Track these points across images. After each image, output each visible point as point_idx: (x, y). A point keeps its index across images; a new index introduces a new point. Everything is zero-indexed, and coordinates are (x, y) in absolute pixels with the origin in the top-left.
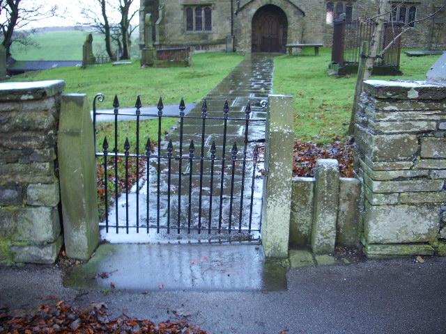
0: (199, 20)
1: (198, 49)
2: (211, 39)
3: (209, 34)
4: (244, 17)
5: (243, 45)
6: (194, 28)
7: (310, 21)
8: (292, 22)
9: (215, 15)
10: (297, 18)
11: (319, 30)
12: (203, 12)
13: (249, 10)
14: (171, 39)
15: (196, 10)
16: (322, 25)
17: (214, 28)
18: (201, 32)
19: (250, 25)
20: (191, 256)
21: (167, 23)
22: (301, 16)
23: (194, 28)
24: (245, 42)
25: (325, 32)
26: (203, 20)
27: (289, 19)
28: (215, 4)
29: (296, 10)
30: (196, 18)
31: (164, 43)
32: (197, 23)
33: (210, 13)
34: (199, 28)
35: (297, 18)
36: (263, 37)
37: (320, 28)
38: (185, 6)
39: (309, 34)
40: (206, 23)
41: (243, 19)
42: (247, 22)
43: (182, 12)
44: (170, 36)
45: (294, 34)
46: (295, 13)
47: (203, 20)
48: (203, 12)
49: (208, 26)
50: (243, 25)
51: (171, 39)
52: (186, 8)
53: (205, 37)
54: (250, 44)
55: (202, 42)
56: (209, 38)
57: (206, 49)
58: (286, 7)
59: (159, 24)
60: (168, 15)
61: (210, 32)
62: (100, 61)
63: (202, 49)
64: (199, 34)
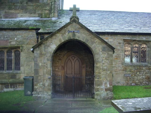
0: (9, 62)
1: (7, 87)
2: (19, 78)
3: (17, 73)
4: (41, 55)
5: (41, 89)
6: (5, 67)
8: (100, 60)
9: (23, 56)
12: (13, 54)
15: (7, 52)
16: (122, 64)
17: (22, 68)
18: (11, 71)
19: (49, 64)
20: (70, 96)
22: (111, 53)
23: (5, 67)
24: (44, 85)
25: (125, 70)
26: (13, 62)
27: (96, 57)
28: (22, 47)
29: (105, 45)
30: (7, 60)
32: (7, 64)
33: (19, 54)
34: (9, 68)
36: (67, 77)
37: (121, 67)
40: (15, 63)
41: (40, 57)
42: (46, 61)
46: (104, 50)
47: (13, 62)
48: (13, 54)
49: (18, 67)
50: (40, 64)
53: (13, 76)
54: (51, 88)
55: (11, 80)
56: (17, 77)
57: (14, 87)
58: (93, 43)
61: (19, 72)
63: (11, 88)
64: (9, 73)
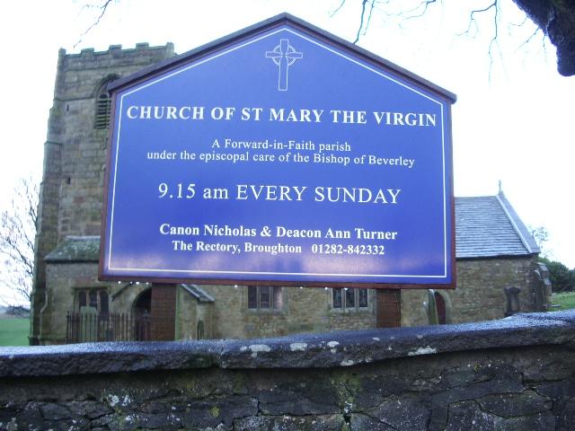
7: (225, 307)
10: (188, 305)
11: (238, 318)
12: (98, 297)
13: (128, 295)
14: (58, 332)
21: (54, 310)
31: (49, 337)
34: (351, 303)
35: (188, 305)
38: (76, 289)
39: (225, 325)
43: (72, 298)
44: (58, 328)
45: (185, 325)
48: (98, 297)
51: (58, 332)
52: (78, 292)
59: (44, 312)
60: (56, 301)
62: (370, 294)
